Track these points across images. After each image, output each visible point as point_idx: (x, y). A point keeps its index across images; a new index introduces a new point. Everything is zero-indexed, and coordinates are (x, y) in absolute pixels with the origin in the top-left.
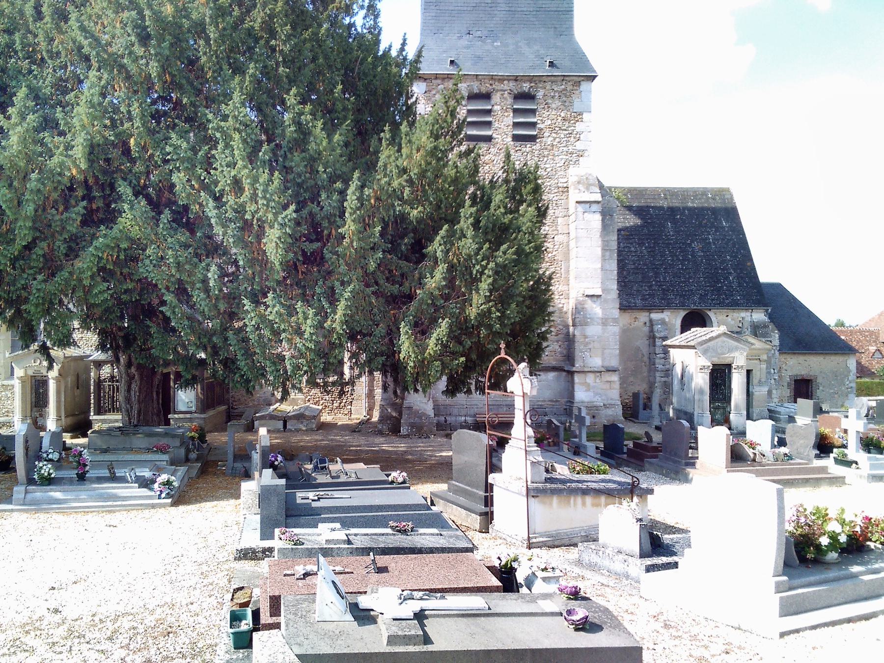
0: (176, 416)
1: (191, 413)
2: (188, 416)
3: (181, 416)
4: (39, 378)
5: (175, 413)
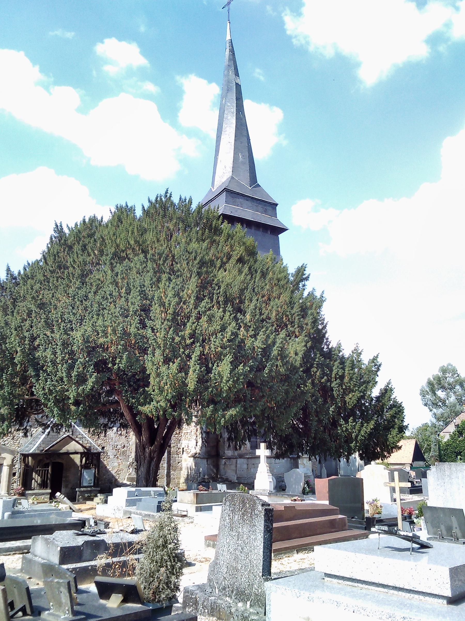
0: (82, 489)
1: (91, 487)
2: (89, 489)
3: (85, 489)
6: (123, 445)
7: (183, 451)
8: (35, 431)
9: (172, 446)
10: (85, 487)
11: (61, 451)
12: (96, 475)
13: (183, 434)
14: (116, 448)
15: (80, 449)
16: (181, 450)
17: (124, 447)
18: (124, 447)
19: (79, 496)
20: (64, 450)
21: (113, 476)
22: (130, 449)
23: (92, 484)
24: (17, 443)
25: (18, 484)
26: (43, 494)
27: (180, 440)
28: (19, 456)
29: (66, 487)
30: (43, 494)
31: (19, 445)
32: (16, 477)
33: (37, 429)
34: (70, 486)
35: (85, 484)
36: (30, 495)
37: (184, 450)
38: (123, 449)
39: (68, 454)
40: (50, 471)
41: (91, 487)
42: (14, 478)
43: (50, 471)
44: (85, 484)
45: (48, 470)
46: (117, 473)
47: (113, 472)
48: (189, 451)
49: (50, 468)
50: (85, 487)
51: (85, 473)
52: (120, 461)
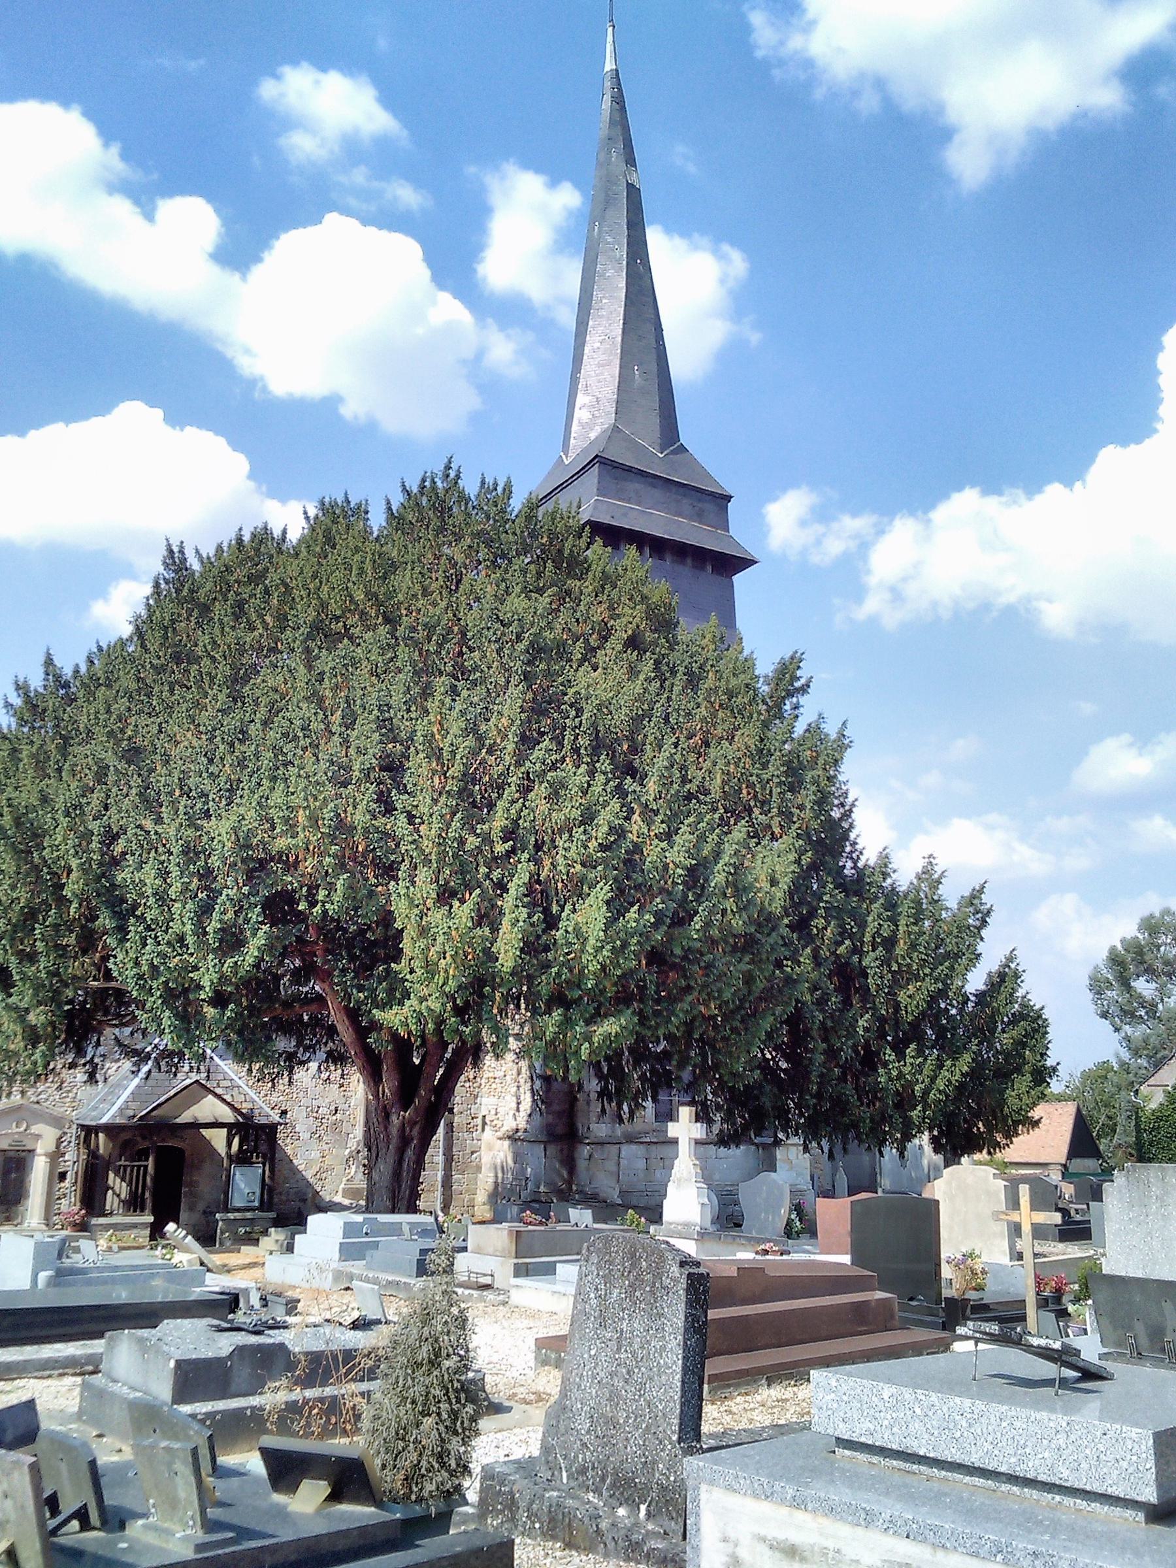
0: (231, 1216)
1: (252, 1209)
2: (249, 1215)
3: (238, 1215)
4: (12, 1154)
5: (227, 1210)
6: (333, 1108)
7: (484, 1124)
8: (114, 1068)
9: (455, 1110)
10: (238, 1210)
11: (178, 1121)
12: (267, 1179)
13: (483, 1081)
14: (315, 1115)
15: (228, 1116)
16: (479, 1121)
17: (336, 1111)
18: (336, 1111)
19: (222, 1233)
20: (186, 1117)
21: (309, 1185)
22: (352, 1116)
23: (256, 1204)
24: (68, 1100)
25: (73, 1200)
26: (135, 1226)
27: (476, 1097)
28: (74, 1131)
29: (191, 1209)
30: (135, 1226)
31: (74, 1104)
32: (67, 1183)
33: (120, 1064)
34: (201, 1206)
35: (237, 1202)
36: (100, 1228)
37: (487, 1120)
38: (334, 1118)
39: (196, 1126)
40: (150, 1169)
41: (252, 1209)
42: (62, 1185)
43: (150, 1169)
44: (237, 1202)
45: (146, 1167)
46: (318, 1177)
47: (308, 1175)
48: (499, 1123)
49: (151, 1162)
50: (238, 1210)
51: (238, 1176)
52: (325, 1147)
